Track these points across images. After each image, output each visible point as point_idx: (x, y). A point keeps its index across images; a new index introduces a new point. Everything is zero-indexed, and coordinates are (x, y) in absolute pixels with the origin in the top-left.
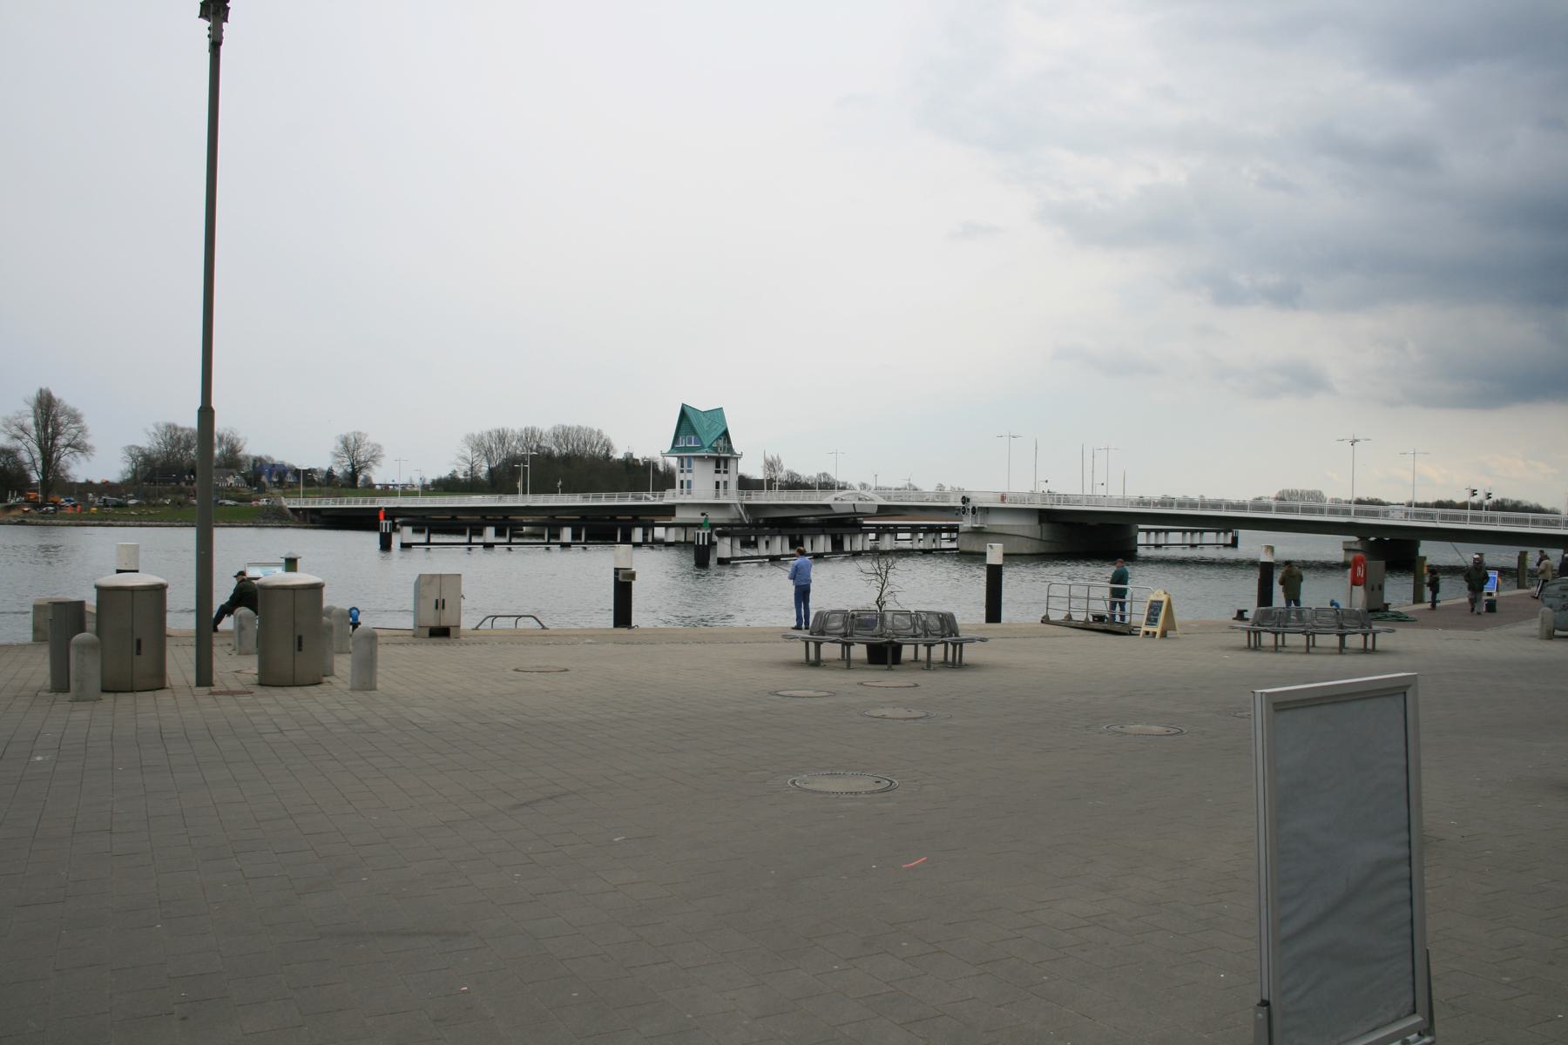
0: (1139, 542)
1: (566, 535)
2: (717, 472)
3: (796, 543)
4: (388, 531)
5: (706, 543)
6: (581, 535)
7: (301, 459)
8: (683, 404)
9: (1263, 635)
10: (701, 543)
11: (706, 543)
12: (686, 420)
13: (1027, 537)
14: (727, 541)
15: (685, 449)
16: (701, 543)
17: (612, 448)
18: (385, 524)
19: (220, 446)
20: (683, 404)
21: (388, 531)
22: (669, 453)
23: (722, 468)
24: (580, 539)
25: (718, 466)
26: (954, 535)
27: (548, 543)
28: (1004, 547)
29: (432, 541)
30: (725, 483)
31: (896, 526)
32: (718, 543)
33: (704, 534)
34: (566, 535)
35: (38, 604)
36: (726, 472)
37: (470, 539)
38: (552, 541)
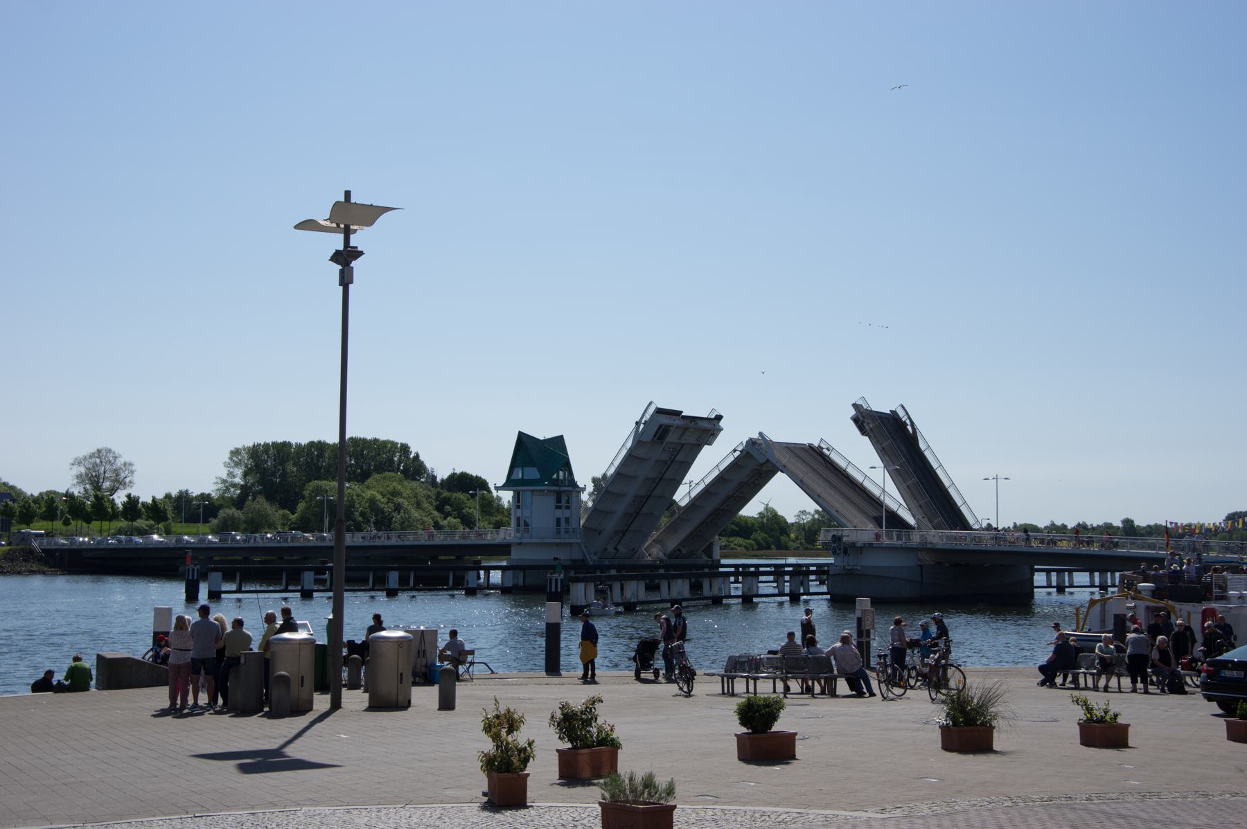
0: (1035, 585)
1: (393, 578)
2: (558, 507)
3: (652, 587)
4: (195, 578)
5: (559, 590)
6: (409, 580)
7: (32, 486)
8: (520, 432)
9: (492, 573)
10: (553, 590)
11: (559, 590)
12: (525, 445)
13: (838, 574)
14: (581, 586)
15: (523, 482)
16: (553, 590)
17: (674, 793)
18: (192, 567)
19: (1240, 710)
20: (520, 432)
21: (195, 578)
22: (504, 485)
23: (563, 504)
24: (409, 584)
25: (559, 500)
26: (825, 577)
27: (286, 590)
28: (399, 573)
29: (243, 589)
30: (567, 520)
31: (757, 566)
32: (134, 493)
33: (556, 580)
34: (393, 578)
35: (309, 600)
36: (568, 508)
37: (240, 586)
38: (290, 588)
